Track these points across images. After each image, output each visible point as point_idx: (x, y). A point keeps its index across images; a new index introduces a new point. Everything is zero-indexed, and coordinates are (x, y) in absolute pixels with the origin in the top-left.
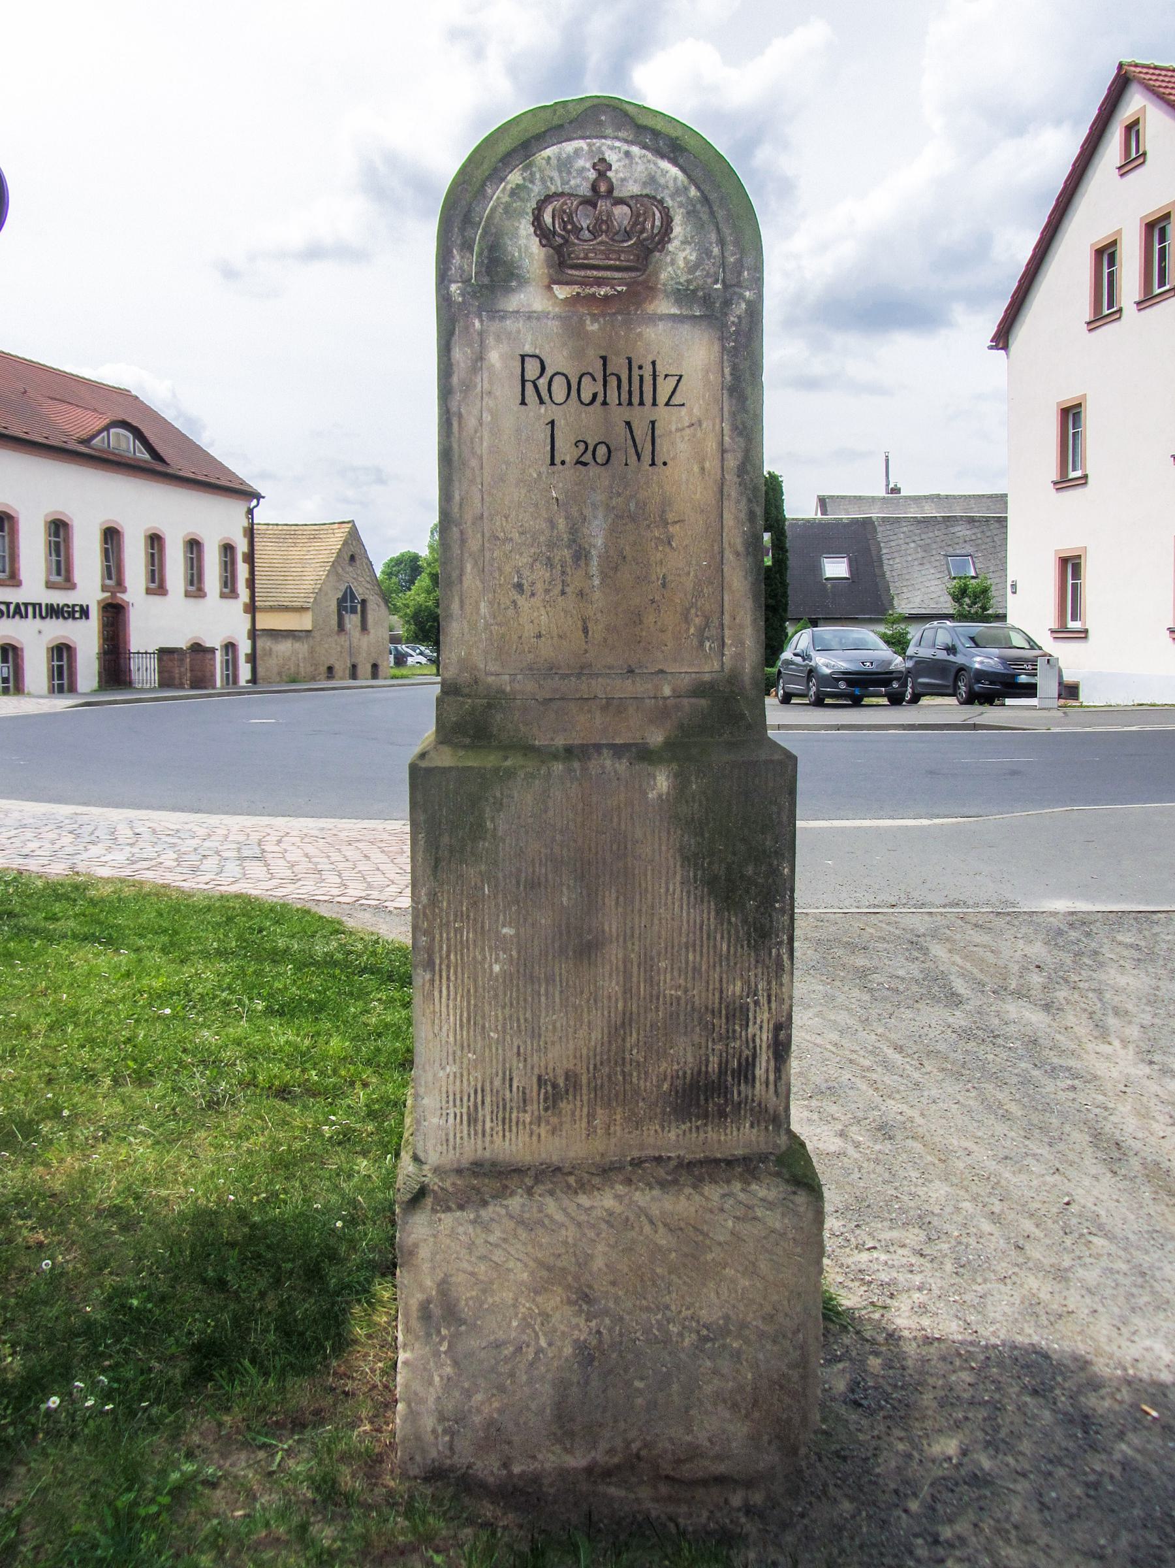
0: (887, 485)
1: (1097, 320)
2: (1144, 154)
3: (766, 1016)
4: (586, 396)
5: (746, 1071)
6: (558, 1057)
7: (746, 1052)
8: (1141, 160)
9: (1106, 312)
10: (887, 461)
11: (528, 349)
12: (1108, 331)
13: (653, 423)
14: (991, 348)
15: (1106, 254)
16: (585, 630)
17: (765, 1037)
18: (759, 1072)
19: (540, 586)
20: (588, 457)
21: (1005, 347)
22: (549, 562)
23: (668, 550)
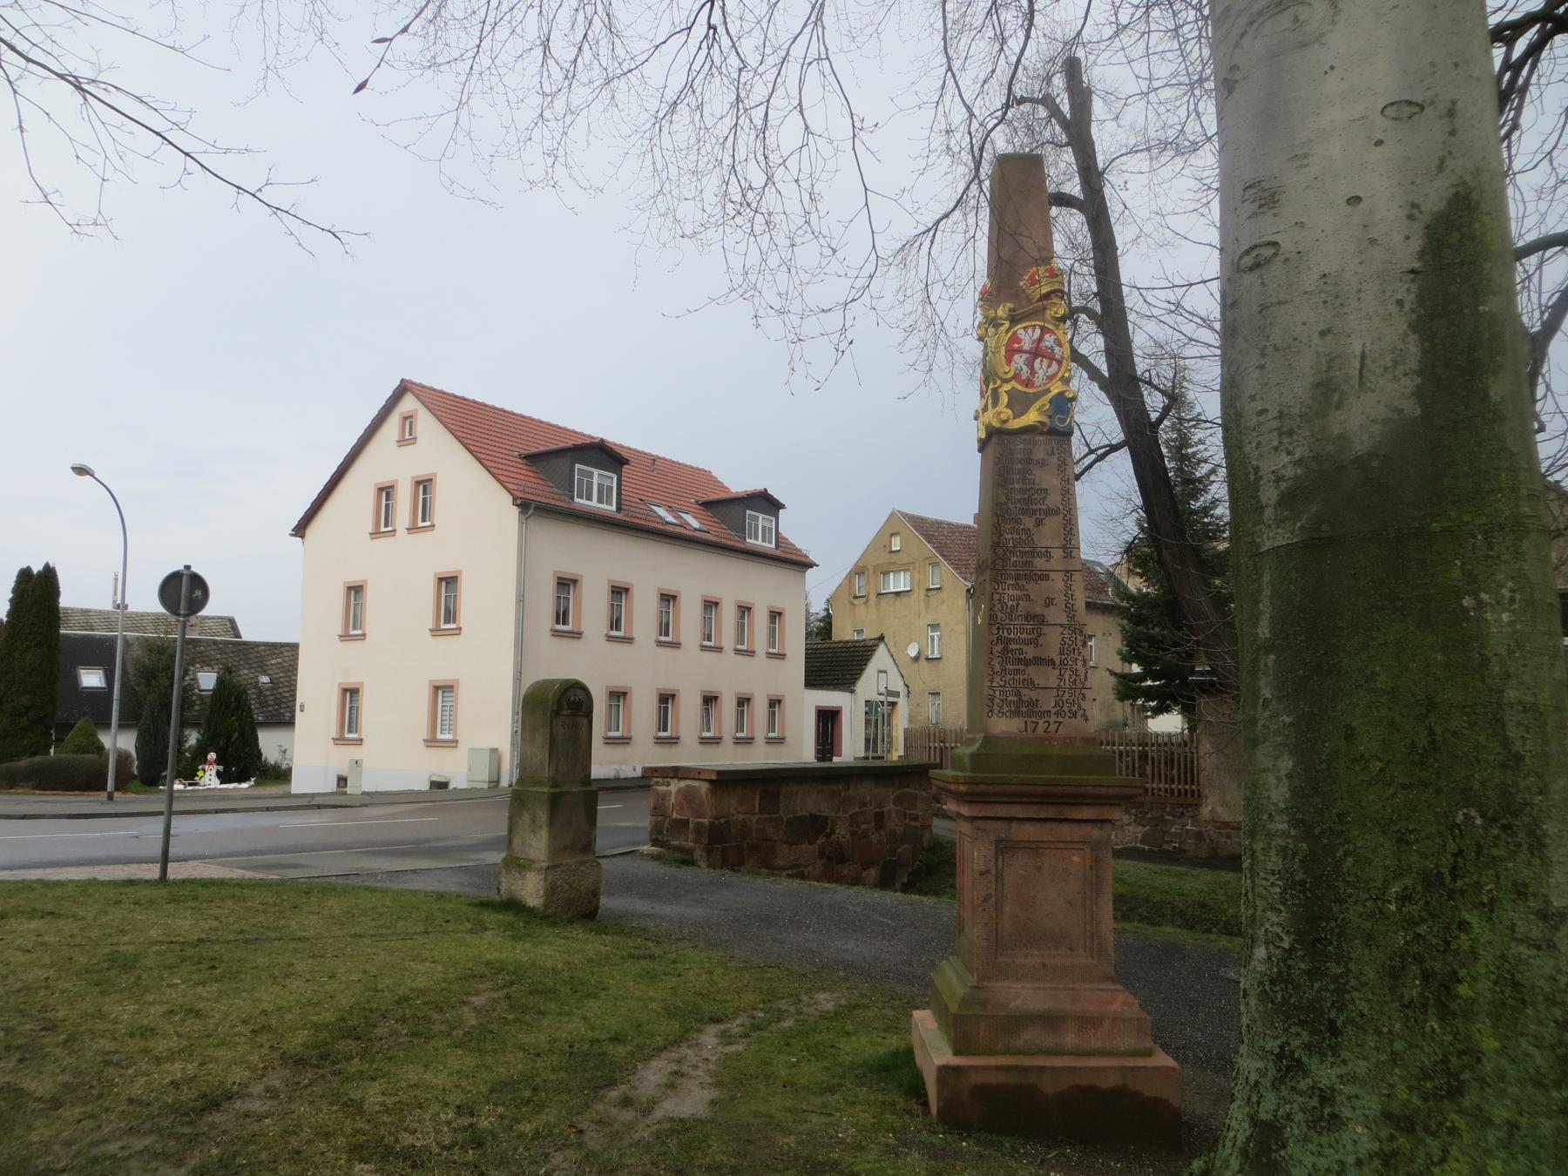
1: (376, 534)
12: (382, 542)
21: (302, 537)
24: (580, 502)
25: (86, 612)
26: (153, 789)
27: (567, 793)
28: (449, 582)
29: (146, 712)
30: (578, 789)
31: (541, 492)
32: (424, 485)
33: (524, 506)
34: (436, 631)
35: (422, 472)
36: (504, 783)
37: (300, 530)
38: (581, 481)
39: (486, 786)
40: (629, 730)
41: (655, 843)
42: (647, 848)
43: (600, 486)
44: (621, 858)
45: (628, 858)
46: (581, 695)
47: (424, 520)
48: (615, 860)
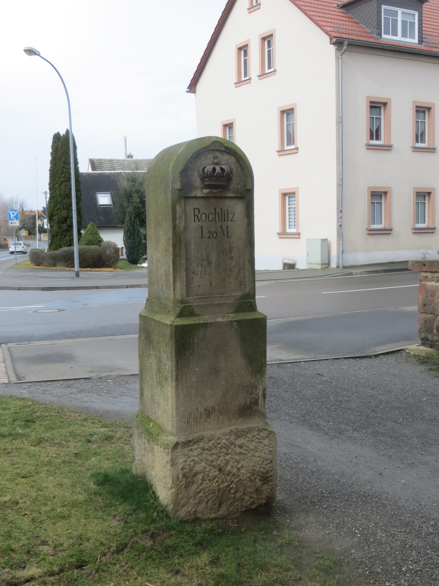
0: (126, 154)
1: (239, 83)
2: (260, 4)
3: (261, 387)
4: (211, 220)
5: (256, 402)
6: (209, 403)
7: (257, 397)
8: (258, 7)
9: (243, 79)
10: (125, 140)
11: (196, 206)
12: (244, 88)
13: (227, 226)
14: (188, 92)
15: (243, 49)
16: (211, 284)
17: (261, 393)
18: (260, 402)
19: (199, 273)
20: (211, 236)
21: (194, 92)
22: (201, 265)
23: (231, 261)
24: (387, 38)
25: (111, 161)
26: (135, 265)
27: (205, 325)
28: (288, 113)
29: (127, 219)
30: (232, 317)
31: (352, 30)
32: (267, 39)
33: (338, 43)
34: (281, 152)
35: (265, 31)
36: (333, 265)
37: (193, 86)
38: (387, 20)
39: (319, 267)
40: (433, 222)
41: (425, 342)
42: (415, 347)
43: (404, 23)
44: (384, 359)
45: (391, 359)
46: (227, 162)
47: (269, 67)
48: (376, 362)
